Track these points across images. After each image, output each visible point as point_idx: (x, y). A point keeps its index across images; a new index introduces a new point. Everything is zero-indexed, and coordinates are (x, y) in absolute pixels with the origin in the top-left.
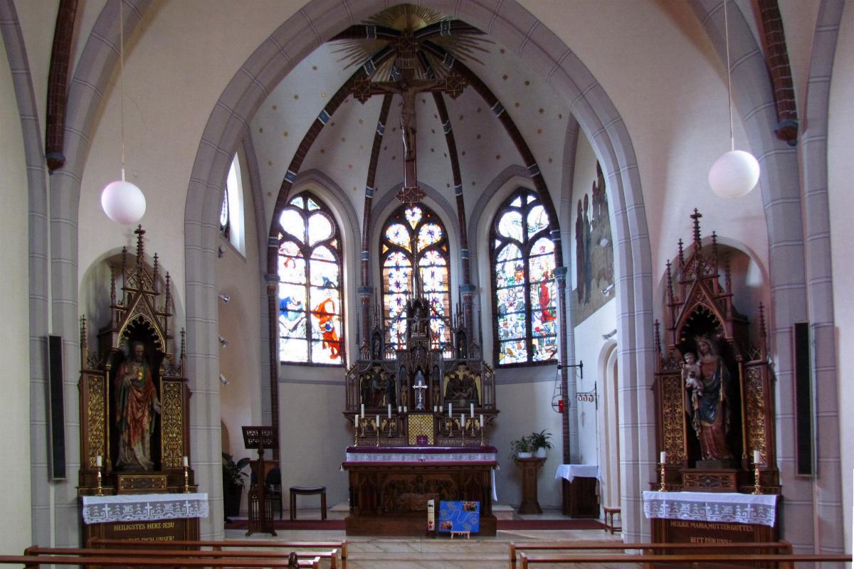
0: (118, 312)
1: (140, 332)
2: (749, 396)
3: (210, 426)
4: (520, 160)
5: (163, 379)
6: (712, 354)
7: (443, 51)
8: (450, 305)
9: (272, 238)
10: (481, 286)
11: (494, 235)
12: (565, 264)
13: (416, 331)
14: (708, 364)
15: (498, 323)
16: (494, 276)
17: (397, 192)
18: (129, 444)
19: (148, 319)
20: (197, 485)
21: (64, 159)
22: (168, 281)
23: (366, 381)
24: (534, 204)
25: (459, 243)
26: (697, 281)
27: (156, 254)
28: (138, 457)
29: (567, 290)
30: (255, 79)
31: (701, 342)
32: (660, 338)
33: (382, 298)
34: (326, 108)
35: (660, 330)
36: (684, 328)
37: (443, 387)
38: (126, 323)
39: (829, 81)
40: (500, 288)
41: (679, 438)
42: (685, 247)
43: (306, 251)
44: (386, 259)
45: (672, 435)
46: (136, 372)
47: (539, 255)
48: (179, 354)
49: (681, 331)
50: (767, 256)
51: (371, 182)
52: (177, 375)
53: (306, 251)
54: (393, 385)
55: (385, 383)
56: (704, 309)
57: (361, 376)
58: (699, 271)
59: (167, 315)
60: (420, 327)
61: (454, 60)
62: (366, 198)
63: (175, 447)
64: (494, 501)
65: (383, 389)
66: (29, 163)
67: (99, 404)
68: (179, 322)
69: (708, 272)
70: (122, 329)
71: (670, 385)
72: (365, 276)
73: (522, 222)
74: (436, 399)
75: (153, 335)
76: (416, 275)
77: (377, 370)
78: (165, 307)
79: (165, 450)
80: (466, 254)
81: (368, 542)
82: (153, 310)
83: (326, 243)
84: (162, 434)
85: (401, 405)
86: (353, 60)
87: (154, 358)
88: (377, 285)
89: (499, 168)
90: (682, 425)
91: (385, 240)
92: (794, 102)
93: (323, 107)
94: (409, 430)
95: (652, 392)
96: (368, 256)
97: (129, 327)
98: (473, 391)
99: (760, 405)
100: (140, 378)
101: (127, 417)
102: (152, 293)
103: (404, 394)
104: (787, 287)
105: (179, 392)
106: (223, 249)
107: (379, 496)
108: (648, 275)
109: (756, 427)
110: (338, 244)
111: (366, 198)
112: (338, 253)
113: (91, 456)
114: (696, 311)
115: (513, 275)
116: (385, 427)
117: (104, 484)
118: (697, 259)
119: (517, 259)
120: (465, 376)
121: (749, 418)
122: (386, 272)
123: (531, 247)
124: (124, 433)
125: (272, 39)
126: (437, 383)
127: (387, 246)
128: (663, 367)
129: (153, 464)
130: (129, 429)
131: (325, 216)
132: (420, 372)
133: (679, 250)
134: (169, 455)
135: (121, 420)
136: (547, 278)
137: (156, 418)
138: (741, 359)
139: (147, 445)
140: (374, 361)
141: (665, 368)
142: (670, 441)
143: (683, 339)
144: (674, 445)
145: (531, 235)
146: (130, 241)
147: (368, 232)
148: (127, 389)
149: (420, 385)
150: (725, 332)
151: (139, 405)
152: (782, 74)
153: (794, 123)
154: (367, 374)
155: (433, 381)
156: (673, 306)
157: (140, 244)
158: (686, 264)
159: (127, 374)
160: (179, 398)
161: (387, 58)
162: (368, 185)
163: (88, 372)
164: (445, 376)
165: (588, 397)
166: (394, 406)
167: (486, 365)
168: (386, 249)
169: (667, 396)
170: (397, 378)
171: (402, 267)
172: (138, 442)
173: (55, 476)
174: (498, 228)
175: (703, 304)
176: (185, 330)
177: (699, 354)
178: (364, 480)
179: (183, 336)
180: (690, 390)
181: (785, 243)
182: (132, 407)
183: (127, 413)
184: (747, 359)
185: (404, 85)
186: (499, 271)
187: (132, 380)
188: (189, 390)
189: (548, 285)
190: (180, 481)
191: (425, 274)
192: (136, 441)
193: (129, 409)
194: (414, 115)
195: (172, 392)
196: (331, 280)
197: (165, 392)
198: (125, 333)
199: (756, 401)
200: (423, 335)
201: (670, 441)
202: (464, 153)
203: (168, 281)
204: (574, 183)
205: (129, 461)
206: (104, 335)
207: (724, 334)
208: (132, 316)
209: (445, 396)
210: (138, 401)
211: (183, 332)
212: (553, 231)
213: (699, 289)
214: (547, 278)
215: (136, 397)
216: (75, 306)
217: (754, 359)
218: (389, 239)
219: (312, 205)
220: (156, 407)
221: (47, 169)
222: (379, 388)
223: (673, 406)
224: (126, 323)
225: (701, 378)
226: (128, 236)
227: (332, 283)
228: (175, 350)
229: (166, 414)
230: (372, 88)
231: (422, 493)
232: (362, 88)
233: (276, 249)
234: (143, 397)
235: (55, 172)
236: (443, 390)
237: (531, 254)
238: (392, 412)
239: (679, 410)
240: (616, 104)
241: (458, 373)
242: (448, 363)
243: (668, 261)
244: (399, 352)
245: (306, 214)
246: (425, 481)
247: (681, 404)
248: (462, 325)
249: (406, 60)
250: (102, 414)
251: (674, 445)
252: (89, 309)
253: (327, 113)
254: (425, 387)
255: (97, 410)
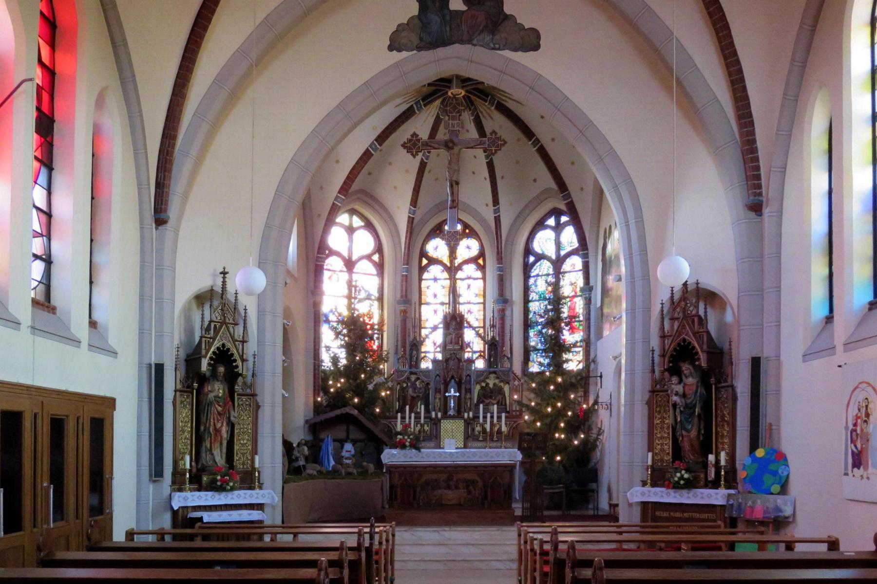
0: (205, 341)
1: (223, 357)
2: (719, 412)
3: (274, 434)
4: (553, 185)
5: (238, 395)
6: (693, 377)
7: (487, 95)
8: (484, 315)
9: (320, 256)
10: (514, 299)
11: (528, 251)
12: (592, 283)
13: (451, 343)
14: (689, 385)
15: (528, 333)
16: (526, 289)
17: (440, 207)
18: (211, 450)
19: (229, 345)
20: (262, 484)
21: (169, 217)
22: (245, 313)
23: (403, 389)
24: (566, 224)
25: (495, 259)
26: (683, 318)
27: (236, 291)
28: (217, 461)
29: (592, 307)
30: (324, 139)
31: (686, 368)
32: (655, 362)
33: (420, 309)
34: (376, 140)
35: (655, 355)
36: (672, 356)
37: (474, 394)
38: (212, 350)
39: (785, 172)
40: (531, 301)
41: (666, 444)
42: (675, 290)
43: (350, 264)
44: (425, 271)
45: (661, 441)
46: (217, 390)
47: (569, 272)
48: (250, 373)
49: (669, 358)
50: (737, 302)
51: (414, 202)
52: (248, 391)
53: (350, 264)
54: (428, 392)
55: (421, 391)
56: (687, 341)
57: (399, 383)
58: (684, 310)
59: (244, 342)
60: (455, 338)
61: (496, 102)
62: (409, 217)
63: (246, 451)
64: (516, 498)
65: (418, 396)
66: (142, 223)
67: (187, 417)
68: (251, 348)
69: (691, 312)
70: (209, 355)
71: (661, 401)
72: (404, 288)
73: (555, 240)
74: (467, 406)
75: (232, 358)
76: (453, 292)
77: (413, 378)
78: (242, 335)
79: (237, 454)
80: (500, 269)
81: (405, 531)
82: (232, 337)
83: (369, 257)
84: (235, 441)
85: (434, 410)
86: (405, 100)
87: (232, 377)
88: (415, 298)
89: (536, 189)
90: (669, 433)
91: (423, 254)
92: (761, 183)
93: (374, 137)
94: (442, 434)
95: (647, 406)
96: (407, 270)
97: (214, 353)
98: (502, 398)
99: (726, 419)
100: (220, 395)
101: (209, 428)
102: (232, 324)
103: (437, 400)
104: (748, 327)
105: (250, 406)
106: (288, 281)
107: (415, 492)
108: (648, 310)
109: (723, 436)
110: (379, 258)
111: (409, 217)
112: (380, 267)
113: (181, 460)
114: (676, 347)
115: (545, 289)
116: (419, 431)
117: (190, 483)
118: (684, 301)
119: (548, 275)
120: (495, 384)
121: (719, 429)
122: (424, 284)
123: (562, 263)
124: (207, 441)
125: (340, 106)
126: (469, 391)
127: (426, 259)
128: (656, 386)
129: (228, 466)
130: (211, 437)
131: (369, 231)
132: (453, 381)
133: (671, 292)
134: (240, 458)
135: (205, 430)
136: (576, 293)
137: (232, 426)
138: (714, 382)
139: (224, 450)
140: (411, 370)
141: (658, 387)
142: (659, 447)
143: (671, 365)
144: (662, 450)
145: (563, 253)
146: (214, 280)
147: (409, 248)
148: (210, 404)
149: (452, 392)
150: (702, 360)
151: (219, 417)
152: (752, 162)
153: (760, 200)
154: (404, 382)
155: (466, 389)
156: (663, 337)
157: (224, 282)
158: (676, 304)
159: (210, 391)
160: (250, 410)
161: (435, 99)
162: (411, 205)
163: (181, 391)
164: (476, 384)
165: (604, 406)
166: (427, 411)
167: (515, 374)
168: (425, 262)
169: (658, 409)
170: (432, 387)
171: (439, 279)
172: (218, 448)
173: (155, 477)
174: (532, 244)
175: (687, 338)
176: (256, 353)
177: (684, 378)
178: (403, 478)
179: (254, 358)
180: (675, 405)
181: (748, 293)
182: (214, 419)
183: (210, 425)
184: (718, 382)
185: (451, 145)
186: (531, 285)
187: (215, 397)
188: (258, 403)
189: (576, 300)
190: (250, 480)
191: (461, 286)
192: (216, 447)
193: (212, 420)
194: (458, 170)
195: (244, 405)
196: (371, 293)
197: (239, 405)
198: (211, 358)
199: (723, 416)
200: (457, 347)
201: (659, 447)
202: (503, 178)
203: (245, 313)
204: (603, 214)
205: (210, 464)
206: (191, 360)
207: (701, 362)
208: (217, 344)
209: (475, 402)
210: (219, 414)
211: (255, 355)
212: (583, 248)
213: (684, 325)
214: (576, 293)
215: (217, 411)
216: (172, 337)
217: (724, 383)
218: (428, 252)
219: (357, 222)
220: (232, 419)
221: (154, 225)
222: (415, 395)
223: (663, 419)
224: (212, 350)
225: (684, 395)
226: (214, 275)
227: (372, 295)
228: (248, 369)
229: (239, 424)
230: (423, 145)
231: (452, 490)
232: (415, 145)
233: (322, 266)
234: (223, 410)
235: (160, 228)
236: (474, 396)
237: (562, 270)
238: (425, 418)
239: (667, 421)
240: (627, 165)
241: (488, 381)
242: (480, 373)
243: (662, 300)
244: (435, 361)
245: (350, 230)
246: (455, 480)
247: (669, 417)
248: (493, 338)
249: (453, 122)
250: (189, 425)
251: (662, 450)
252: (180, 340)
253: (377, 144)
254: (458, 394)
255: (186, 422)
